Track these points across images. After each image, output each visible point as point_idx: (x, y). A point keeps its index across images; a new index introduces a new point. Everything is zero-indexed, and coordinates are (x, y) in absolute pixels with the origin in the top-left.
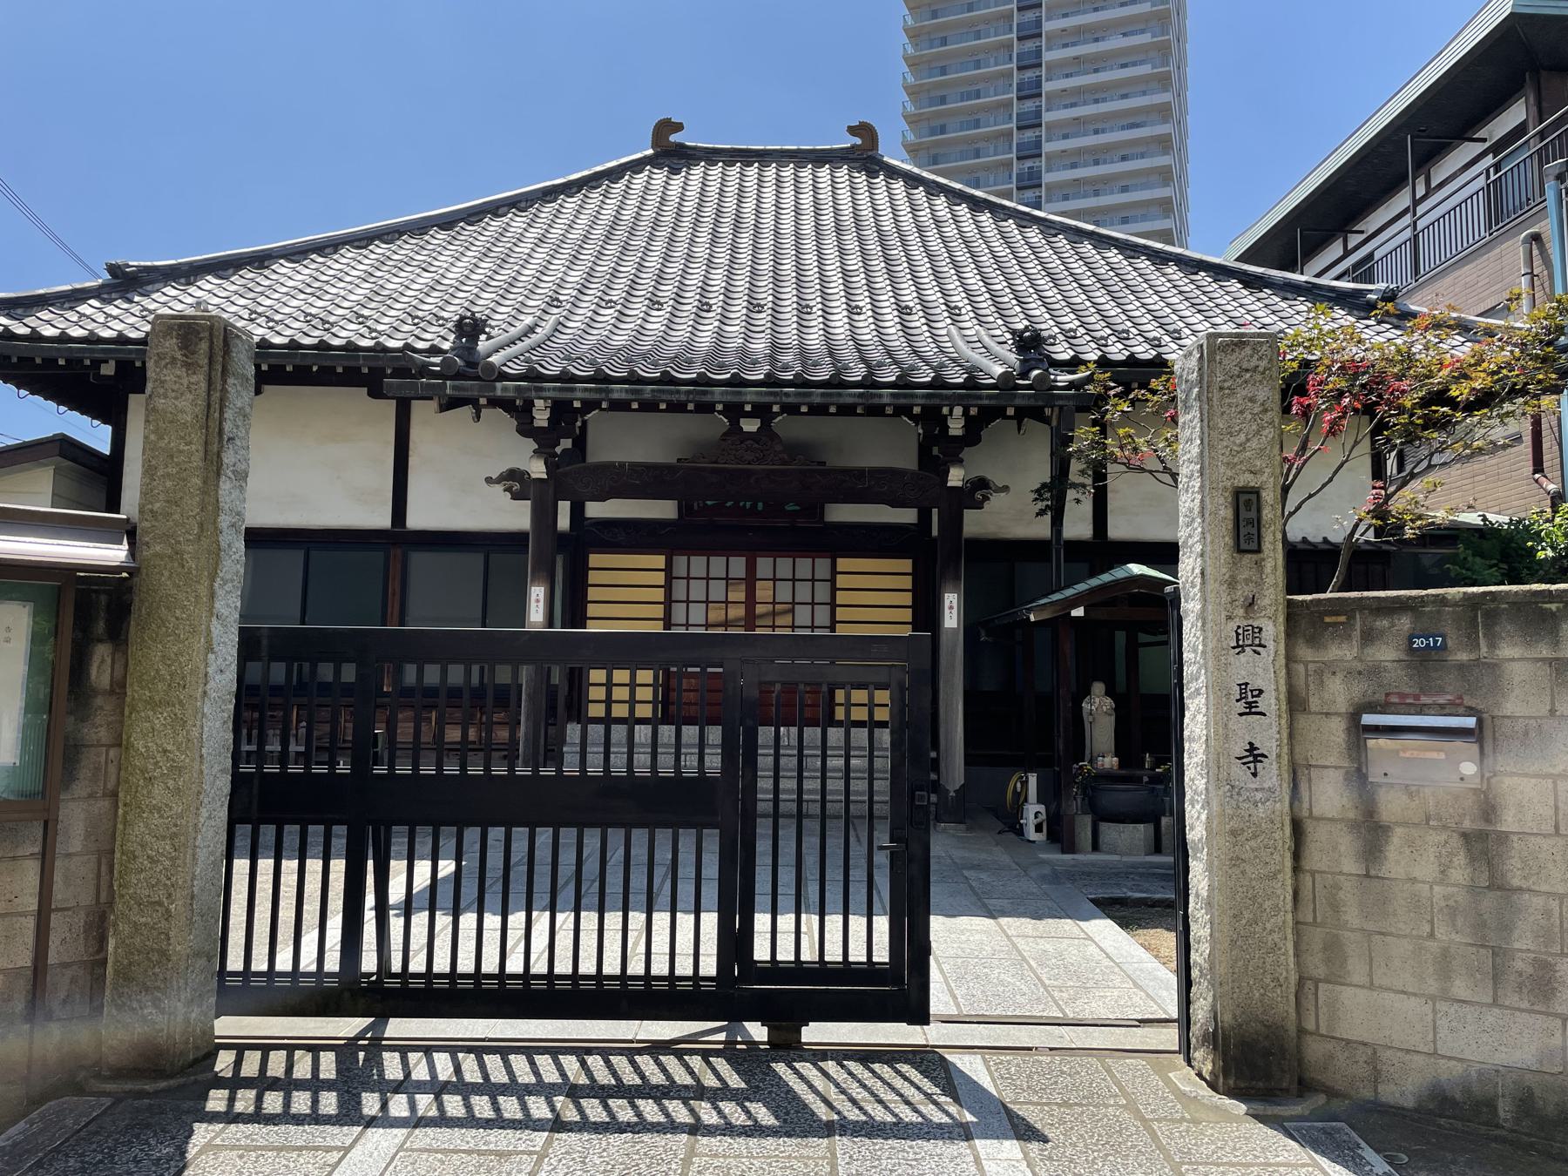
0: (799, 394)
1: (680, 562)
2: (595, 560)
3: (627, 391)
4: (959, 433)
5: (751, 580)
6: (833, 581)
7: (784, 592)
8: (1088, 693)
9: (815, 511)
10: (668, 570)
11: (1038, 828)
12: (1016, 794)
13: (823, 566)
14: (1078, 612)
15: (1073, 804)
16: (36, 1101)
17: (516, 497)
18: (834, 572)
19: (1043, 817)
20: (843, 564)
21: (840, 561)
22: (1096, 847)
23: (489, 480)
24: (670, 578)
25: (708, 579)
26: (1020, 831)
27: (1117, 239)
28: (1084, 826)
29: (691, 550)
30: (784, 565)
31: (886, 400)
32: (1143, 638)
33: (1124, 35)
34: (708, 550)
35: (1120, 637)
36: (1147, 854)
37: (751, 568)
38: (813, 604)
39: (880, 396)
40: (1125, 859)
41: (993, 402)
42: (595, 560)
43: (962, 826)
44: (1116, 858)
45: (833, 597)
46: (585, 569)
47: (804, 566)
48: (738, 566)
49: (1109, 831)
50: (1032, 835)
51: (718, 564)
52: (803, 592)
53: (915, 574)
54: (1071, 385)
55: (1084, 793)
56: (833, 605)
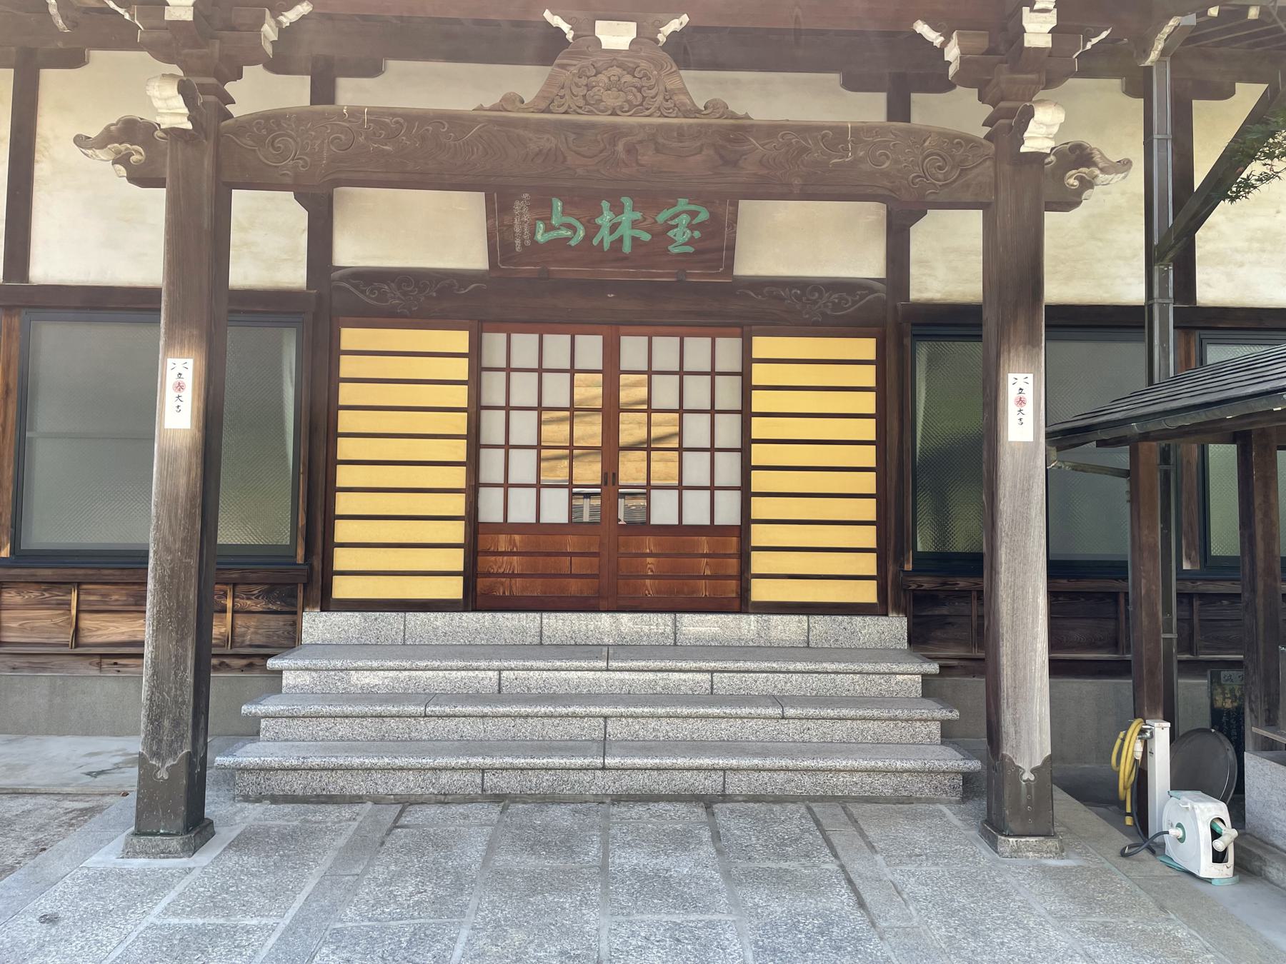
1: (494, 344)
2: (351, 337)
4: (1045, 42)
5: (611, 371)
9: (718, 242)
10: (475, 354)
16: (672, 577)
17: (142, 177)
18: (748, 360)
20: (763, 346)
21: (757, 341)
23: (81, 141)
24: (477, 369)
25: (540, 370)
29: (512, 323)
30: (666, 350)
34: (541, 324)
38: (712, 450)
42: (351, 337)
46: (334, 352)
47: (698, 351)
48: (591, 349)
51: (557, 345)
52: (697, 393)
53: (880, 362)
56: (746, 414)
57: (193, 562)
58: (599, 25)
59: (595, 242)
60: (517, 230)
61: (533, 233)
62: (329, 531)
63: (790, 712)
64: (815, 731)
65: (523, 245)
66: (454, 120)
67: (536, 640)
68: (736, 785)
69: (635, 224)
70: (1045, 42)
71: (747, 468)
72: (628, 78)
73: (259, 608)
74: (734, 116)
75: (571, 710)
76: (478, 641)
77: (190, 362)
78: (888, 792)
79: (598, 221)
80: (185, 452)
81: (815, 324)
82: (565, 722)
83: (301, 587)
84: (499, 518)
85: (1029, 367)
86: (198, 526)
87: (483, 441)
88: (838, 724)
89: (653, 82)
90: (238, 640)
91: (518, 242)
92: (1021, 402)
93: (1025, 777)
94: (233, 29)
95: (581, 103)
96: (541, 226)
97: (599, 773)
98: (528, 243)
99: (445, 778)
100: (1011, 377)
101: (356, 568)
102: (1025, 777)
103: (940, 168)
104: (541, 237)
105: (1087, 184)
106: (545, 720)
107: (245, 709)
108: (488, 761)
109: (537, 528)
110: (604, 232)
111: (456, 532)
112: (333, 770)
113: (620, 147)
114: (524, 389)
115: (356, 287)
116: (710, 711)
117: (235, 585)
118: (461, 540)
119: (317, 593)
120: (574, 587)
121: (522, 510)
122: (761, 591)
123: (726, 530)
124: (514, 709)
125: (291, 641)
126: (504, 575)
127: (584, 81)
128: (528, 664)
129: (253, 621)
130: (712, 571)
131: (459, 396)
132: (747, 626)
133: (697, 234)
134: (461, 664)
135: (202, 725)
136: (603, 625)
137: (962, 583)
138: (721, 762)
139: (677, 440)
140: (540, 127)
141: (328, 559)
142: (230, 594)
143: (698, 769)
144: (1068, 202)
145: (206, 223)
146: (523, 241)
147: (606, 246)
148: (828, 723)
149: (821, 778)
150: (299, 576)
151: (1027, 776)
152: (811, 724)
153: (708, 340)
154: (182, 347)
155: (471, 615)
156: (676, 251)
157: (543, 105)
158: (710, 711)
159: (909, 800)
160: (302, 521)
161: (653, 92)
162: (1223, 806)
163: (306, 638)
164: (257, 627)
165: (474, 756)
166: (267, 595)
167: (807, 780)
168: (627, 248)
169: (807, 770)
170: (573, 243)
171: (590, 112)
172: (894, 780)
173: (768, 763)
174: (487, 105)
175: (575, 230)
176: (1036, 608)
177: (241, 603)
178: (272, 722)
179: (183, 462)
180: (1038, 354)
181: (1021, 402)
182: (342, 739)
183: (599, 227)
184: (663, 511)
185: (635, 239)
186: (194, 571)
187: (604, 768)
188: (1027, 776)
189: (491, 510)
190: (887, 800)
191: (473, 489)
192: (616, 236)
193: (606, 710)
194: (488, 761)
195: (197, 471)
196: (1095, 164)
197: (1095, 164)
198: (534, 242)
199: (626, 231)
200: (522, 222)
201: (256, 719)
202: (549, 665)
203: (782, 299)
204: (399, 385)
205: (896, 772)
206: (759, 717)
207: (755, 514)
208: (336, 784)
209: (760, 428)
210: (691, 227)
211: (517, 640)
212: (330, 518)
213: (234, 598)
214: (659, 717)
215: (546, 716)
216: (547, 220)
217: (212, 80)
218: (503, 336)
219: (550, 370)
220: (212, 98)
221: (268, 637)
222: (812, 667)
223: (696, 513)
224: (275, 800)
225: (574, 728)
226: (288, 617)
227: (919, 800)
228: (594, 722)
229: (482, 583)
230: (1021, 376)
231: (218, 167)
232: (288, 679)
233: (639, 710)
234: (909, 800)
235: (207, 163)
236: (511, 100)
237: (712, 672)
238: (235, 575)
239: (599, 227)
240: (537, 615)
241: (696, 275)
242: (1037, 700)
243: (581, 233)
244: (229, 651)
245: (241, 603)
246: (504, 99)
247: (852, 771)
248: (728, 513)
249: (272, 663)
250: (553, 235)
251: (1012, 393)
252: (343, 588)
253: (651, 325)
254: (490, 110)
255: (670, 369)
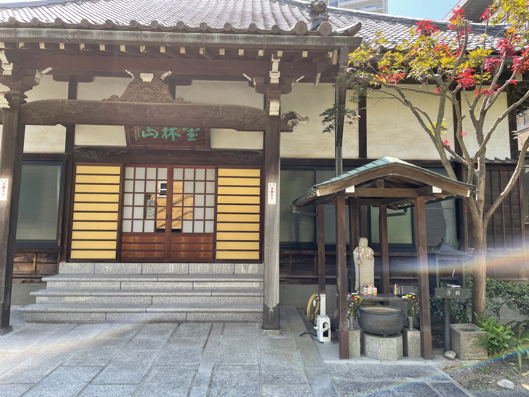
0: (154, 35)
2: (80, 169)
3: (29, 32)
4: (277, 81)
6: (216, 181)
7: (189, 187)
8: (357, 245)
10: (123, 175)
11: (325, 334)
12: (313, 308)
13: (211, 173)
14: (351, 190)
15: (348, 323)
18: (217, 176)
19: (328, 327)
20: (222, 172)
22: (363, 352)
26: (314, 334)
27: (370, 15)
28: (355, 337)
29: (136, 164)
30: (189, 173)
31: (217, 41)
32: (389, 211)
33: (367, 7)
34: (146, 164)
35: (375, 212)
36: (398, 359)
37: (171, 174)
38: (205, 207)
39: (213, 38)
40: (384, 363)
41: (292, 43)
42: (80, 169)
43: (277, 331)
44: (377, 362)
45: (216, 190)
47: (200, 173)
48: (163, 173)
49: (372, 342)
50: (321, 338)
54: (346, 33)
55: (355, 315)
56: (216, 195)
57: (6, 243)
58: (141, 74)
59: (162, 137)
60: (136, 133)
61: (141, 134)
62: (70, 235)
63: (214, 294)
64: (222, 300)
65: (138, 138)
66: (96, 104)
67: (140, 273)
68: (190, 317)
69: (175, 131)
70: (277, 81)
71: (216, 213)
72: (151, 91)
73: (45, 262)
74: (185, 102)
75: (140, 294)
76: (120, 273)
77: (7, 180)
78: (241, 319)
79: (163, 130)
80: (5, 209)
81: (239, 165)
82: (138, 298)
83: (59, 255)
84: (129, 231)
85: (275, 181)
86: (8, 232)
87: (125, 204)
88: (230, 298)
89: (159, 92)
90: (37, 272)
91: (136, 137)
92: (272, 192)
93: (271, 310)
94: (27, 76)
95: (136, 98)
96: (143, 132)
97: (144, 313)
98: (139, 137)
99: (93, 315)
100: (269, 184)
101: (79, 248)
102: (271, 310)
103: (249, 119)
104: (144, 136)
105: (294, 124)
106: (132, 297)
107: (31, 293)
108: (107, 310)
109: (143, 234)
110: (165, 134)
111: (114, 235)
112: (56, 312)
113: (148, 112)
114: (140, 187)
115: (82, 152)
116: (187, 294)
117: (37, 254)
118: (116, 238)
119: (65, 256)
120: (156, 254)
121: (138, 228)
122: (220, 255)
123: (209, 234)
124: (124, 294)
125: (55, 272)
126: (131, 250)
127: (137, 91)
128: (130, 279)
129: (43, 266)
130: (201, 249)
131: (117, 189)
132: (216, 267)
133: (197, 135)
134: (107, 279)
135: (9, 294)
136: (172, 267)
137: (287, 252)
138: (185, 310)
139: (181, 203)
140: (123, 106)
141: (69, 245)
142: (35, 257)
143: (178, 312)
144: (289, 130)
145: (14, 136)
146: (138, 137)
147: (166, 139)
148: (227, 298)
149: (219, 314)
150: (59, 250)
151: (271, 310)
152: (221, 298)
153: (193, 170)
154: (5, 173)
155: (117, 264)
156: (190, 140)
157: (124, 99)
158: (187, 294)
159: (247, 322)
160: (60, 232)
161: (159, 95)
162: (329, 319)
163: (60, 272)
164: (44, 268)
165: (103, 308)
166: (48, 257)
167: (214, 315)
168: (173, 139)
169: (213, 312)
170: (155, 137)
171: (139, 101)
172: (242, 315)
173: (201, 310)
174: (106, 99)
175: (155, 134)
176: (275, 257)
177: (39, 260)
178: (40, 297)
179: (4, 211)
180: (278, 177)
181: (272, 192)
182: (63, 303)
183: (163, 132)
184: (187, 228)
185: (176, 136)
186: (6, 246)
187: (146, 312)
188: (271, 310)
189: (127, 227)
190: (240, 322)
191: (121, 221)
192: (169, 135)
193: (152, 294)
194: (107, 310)
195: (8, 214)
196: (297, 118)
197: (297, 118)
198: (142, 137)
199: (172, 134)
200: (137, 131)
201: (35, 297)
202: (137, 280)
203: (227, 156)
204: (96, 186)
205: (243, 312)
206: (204, 296)
207: (218, 229)
208: (58, 317)
209: (220, 199)
210: (195, 133)
211: (134, 272)
212: (71, 231)
213: (36, 258)
214: (170, 296)
215: (131, 296)
216: (145, 130)
217: (19, 92)
218: (133, 168)
219: (148, 178)
220: (18, 98)
221: (48, 271)
222: (227, 280)
223: (199, 228)
224: (37, 322)
225: (141, 300)
226: (54, 264)
227: (251, 322)
228: (148, 298)
229: (123, 253)
230: (272, 184)
231: (19, 119)
232: (49, 285)
233: (163, 294)
234: (247, 322)
235: (16, 118)
236: (114, 97)
237: (193, 282)
238: (37, 250)
239: (163, 132)
240: (141, 264)
241: (198, 148)
242: (275, 286)
243: (157, 134)
244: (34, 276)
245: (39, 260)
246: (111, 97)
247: (229, 312)
248: (209, 229)
249: (44, 279)
250: (148, 135)
251: (269, 189)
252: (74, 255)
253: (184, 165)
254: (107, 100)
255: (189, 180)
